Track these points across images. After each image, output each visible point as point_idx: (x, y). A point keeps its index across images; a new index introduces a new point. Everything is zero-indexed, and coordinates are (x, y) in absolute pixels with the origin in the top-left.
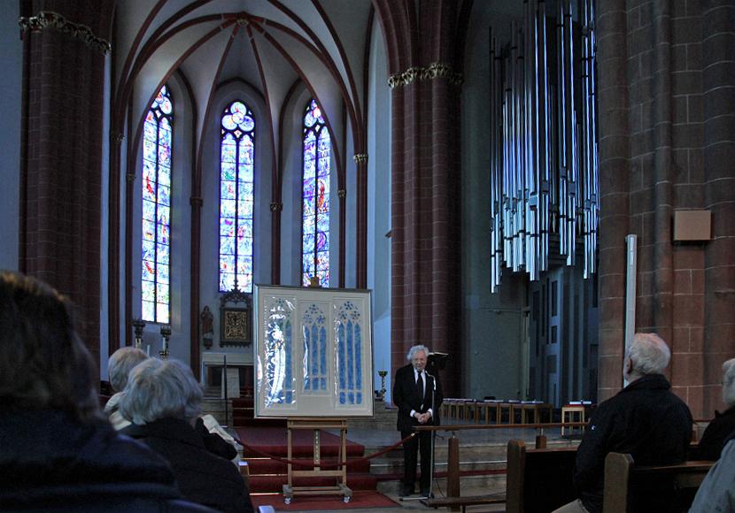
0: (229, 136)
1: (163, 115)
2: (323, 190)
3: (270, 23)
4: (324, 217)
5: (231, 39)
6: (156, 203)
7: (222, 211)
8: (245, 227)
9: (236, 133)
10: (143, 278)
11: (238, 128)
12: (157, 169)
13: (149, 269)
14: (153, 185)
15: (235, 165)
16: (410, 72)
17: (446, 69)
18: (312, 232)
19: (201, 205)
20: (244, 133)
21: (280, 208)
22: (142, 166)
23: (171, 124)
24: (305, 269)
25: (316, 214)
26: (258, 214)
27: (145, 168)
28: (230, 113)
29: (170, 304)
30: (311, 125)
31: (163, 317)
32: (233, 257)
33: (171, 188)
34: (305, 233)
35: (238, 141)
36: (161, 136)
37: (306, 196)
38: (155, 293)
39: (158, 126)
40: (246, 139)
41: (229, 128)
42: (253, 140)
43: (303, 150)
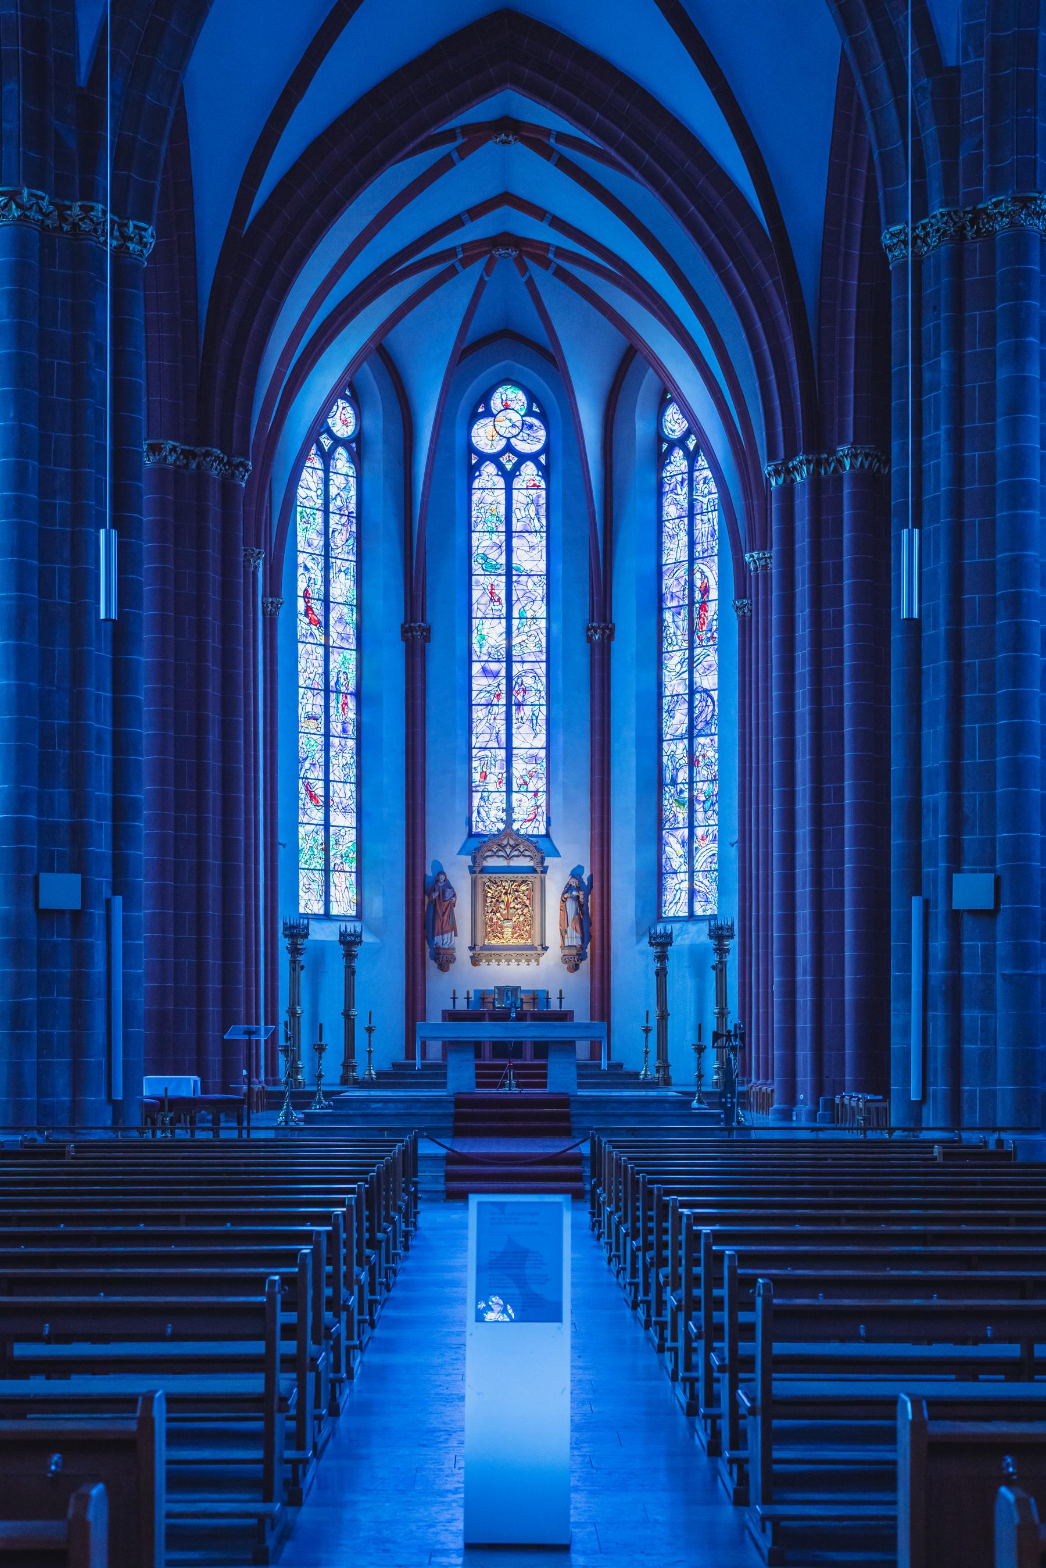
0: (489, 469)
1: (338, 442)
2: (705, 591)
3: (561, 137)
4: (709, 656)
5: (481, 284)
6: (327, 647)
7: (476, 647)
8: (528, 681)
9: (503, 460)
10: (302, 818)
11: (509, 448)
12: (327, 568)
13: (313, 797)
14: (318, 607)
15: (503, 537)
16: (801, 462)
17: (866, 456)
18: (682, 689)
19: (427, 639)
20: (523, 458)
21: (609, 634)
22: (296, 566)
23: (357, 458)
24: (668, 776)
25: (691, 648)
26: (558, 651)
27: (300, 570)
28: (489, 413)
29: (359, 872)
30: (678, 434)
31: (344, 899)
32: (502, 753)
33: (359, 607)
34: (667, 692)
35: (509, 477)
36: (333, 491)
37: (669, 604)
38: (327, 850)
39: (326, 471)
40: (529, 470)
41: (487, 450)
42: (546, 471)
43: (660, 494)
